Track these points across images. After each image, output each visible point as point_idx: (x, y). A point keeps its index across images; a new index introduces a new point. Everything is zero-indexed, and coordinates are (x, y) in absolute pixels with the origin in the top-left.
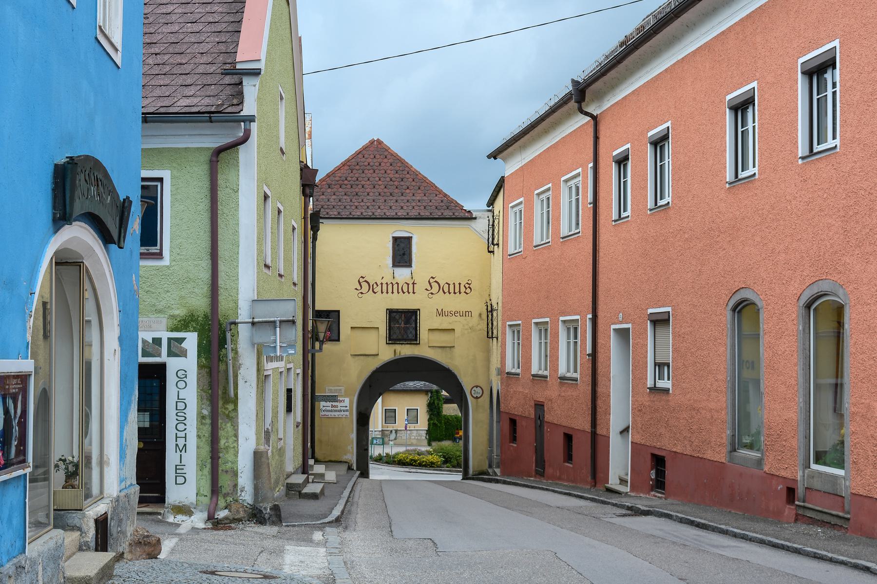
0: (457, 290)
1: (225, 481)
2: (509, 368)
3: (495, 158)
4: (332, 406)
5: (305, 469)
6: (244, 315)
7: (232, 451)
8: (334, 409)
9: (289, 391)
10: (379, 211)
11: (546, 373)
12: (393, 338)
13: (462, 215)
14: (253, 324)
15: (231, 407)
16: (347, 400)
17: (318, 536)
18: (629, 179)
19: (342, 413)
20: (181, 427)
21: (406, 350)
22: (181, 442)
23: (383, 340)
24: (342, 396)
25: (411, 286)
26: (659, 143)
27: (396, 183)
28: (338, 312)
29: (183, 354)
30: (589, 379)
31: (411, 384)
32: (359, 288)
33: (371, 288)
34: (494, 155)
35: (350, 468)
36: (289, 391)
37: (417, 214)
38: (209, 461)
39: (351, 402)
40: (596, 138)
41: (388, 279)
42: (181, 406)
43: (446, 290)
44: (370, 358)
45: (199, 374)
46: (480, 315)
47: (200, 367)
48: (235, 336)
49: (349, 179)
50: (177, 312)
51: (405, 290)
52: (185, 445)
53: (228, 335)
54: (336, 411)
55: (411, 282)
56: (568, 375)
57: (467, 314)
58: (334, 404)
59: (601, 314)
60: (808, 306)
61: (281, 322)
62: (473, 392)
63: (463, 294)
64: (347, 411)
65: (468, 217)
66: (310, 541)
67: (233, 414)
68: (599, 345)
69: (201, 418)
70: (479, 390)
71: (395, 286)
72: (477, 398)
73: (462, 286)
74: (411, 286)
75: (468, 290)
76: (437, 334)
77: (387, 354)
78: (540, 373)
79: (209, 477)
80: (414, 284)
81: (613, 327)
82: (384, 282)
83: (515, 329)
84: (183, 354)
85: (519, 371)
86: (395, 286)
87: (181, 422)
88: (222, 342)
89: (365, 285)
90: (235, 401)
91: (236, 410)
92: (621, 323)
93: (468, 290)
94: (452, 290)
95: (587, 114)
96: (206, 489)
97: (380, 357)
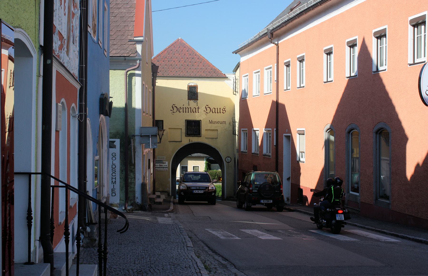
0: (219, 111)
1: (130, 195)
2: (242, 149)
3: (236, 53)
4: (160, 165)
5: (154, 193)
6: (137, 133)
7: (133, 184)
8: (161, 167)
9: (149, 160)
10: (182, 73)
11: (258, 153)
12: (188, 134)
13: (221, 76)
14: (141, 136)
15: (132, 167)
16: (167, 163)
17: (166, 215)
18: (290, 73)
19: (165, 169)
20: (114, 174)
21: (195, 140)
22: (114, 180)
23: (184, 135)
24: (165, 161)
25: (197, 109)
26: (301, 60)
27: (190, 60)
28: (163, 121)
29: (114, 147)
30: (275, 156)
31: (196, 155)
32: (172, 110)
33: (178, 110)
34: (236, 52)
35: (169, 195)
36: (149, 160)
37: (200, 75)
38: (124, 187)
39: (169, 164)
40: (278, 54)
41: (186, 106)
42: (114, 166)
43: (214, 111)
44: (178, 143)
45: (120, 154)
46: (230, 123)
47: (121, 152)
48: (134, 141)
49: (167, 57)
50: (112, 131)
51: (194, 111)
52: (115, 181)
53: (132, 140)
54: (162, 168)
55: (197, 107)
56: (267, 154)
57: (224, 122)
58: (162, 164)
59: (279, 128)
60: (349, 132)
61: (152, 136)
62: (226, 160)
63: (222, 113)
64: (167, 168)
65: (224, 77)
66: (164, 217)
67: (133, 170)
68: (279, 142)
69: (121, 171)
70: (229, 159)
71: (190, 109)
72: (228, 162)
73: (221, 109)
74: (197, 109)
75: (224, 112)
76: (209, 132)
77: (186, 141)
78: (256, 152)
79: (124, 194)
80: (198, 108)
81: (284, 135)
82: (184, 107)
83: (245, 132)
84: (114, 147)
85: (247, 151)
86: (190, 109)
87: (114, 173)
88: (130, 143)
89: (175, 109)
90: (134, 165)
91: (134, 168)
92: (287, 133)
93: (224, 112)
94: (216, 111)
95: (273, 43)
96: (124, 198)
97: (182, 142)
